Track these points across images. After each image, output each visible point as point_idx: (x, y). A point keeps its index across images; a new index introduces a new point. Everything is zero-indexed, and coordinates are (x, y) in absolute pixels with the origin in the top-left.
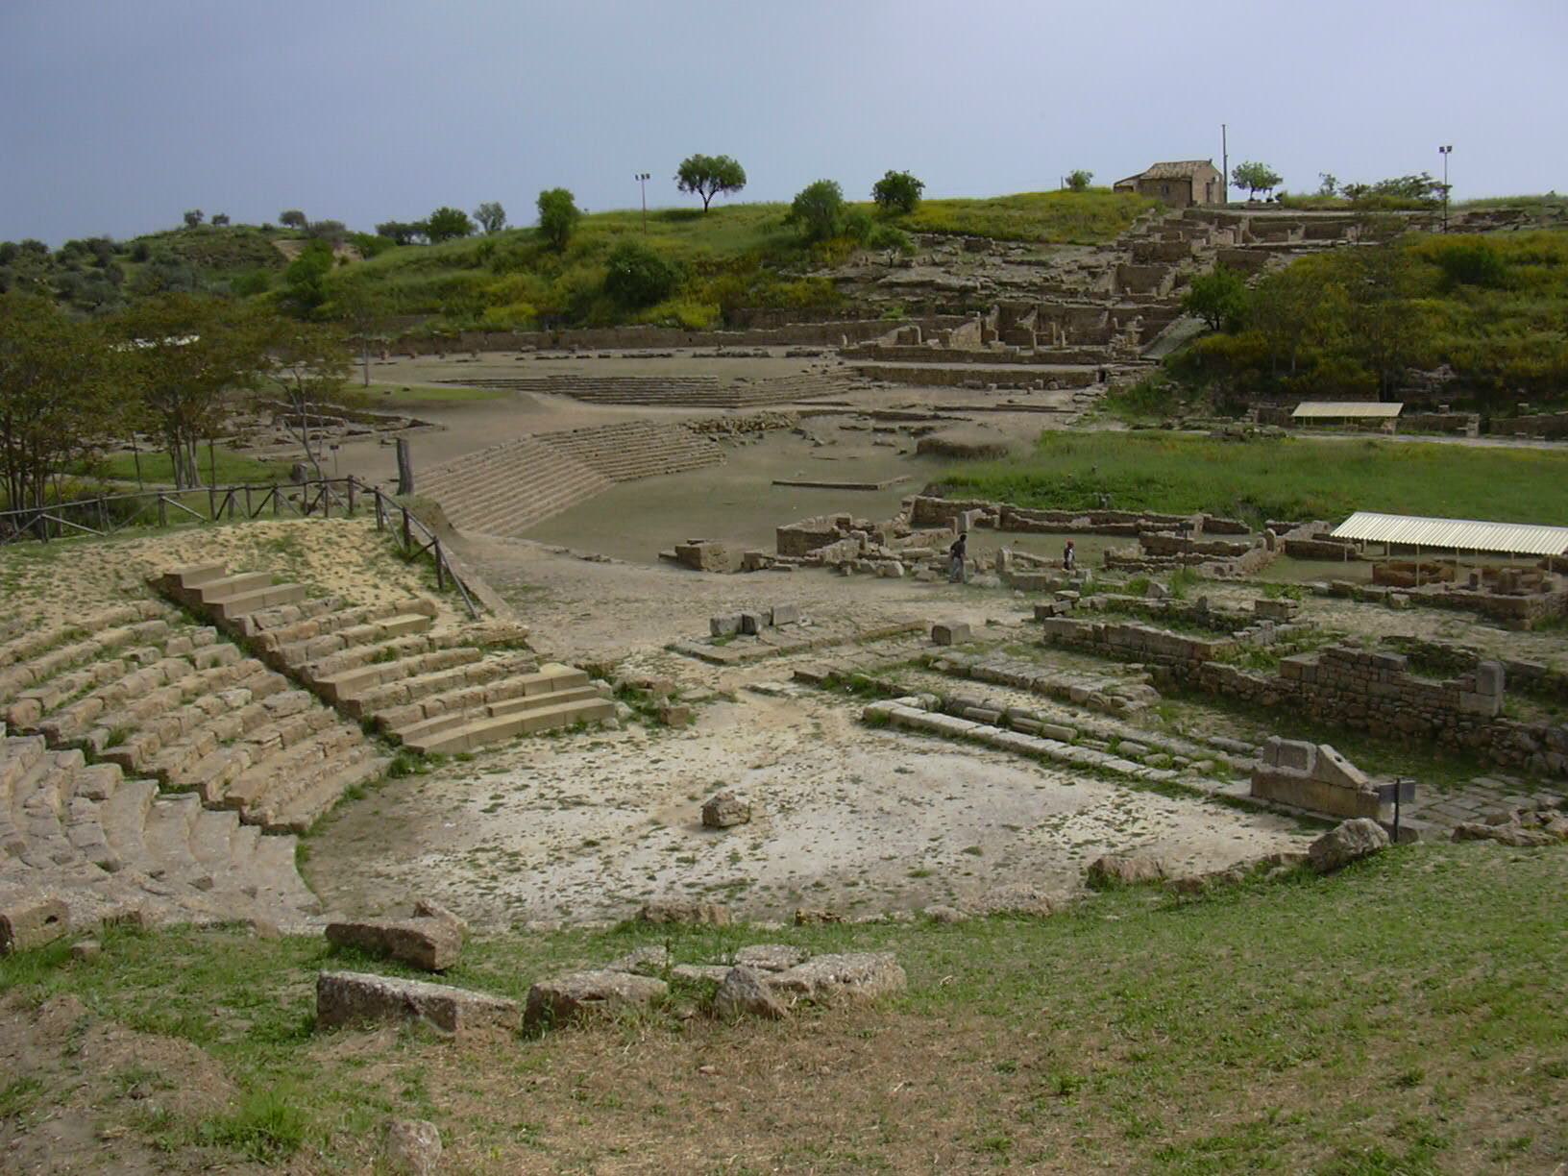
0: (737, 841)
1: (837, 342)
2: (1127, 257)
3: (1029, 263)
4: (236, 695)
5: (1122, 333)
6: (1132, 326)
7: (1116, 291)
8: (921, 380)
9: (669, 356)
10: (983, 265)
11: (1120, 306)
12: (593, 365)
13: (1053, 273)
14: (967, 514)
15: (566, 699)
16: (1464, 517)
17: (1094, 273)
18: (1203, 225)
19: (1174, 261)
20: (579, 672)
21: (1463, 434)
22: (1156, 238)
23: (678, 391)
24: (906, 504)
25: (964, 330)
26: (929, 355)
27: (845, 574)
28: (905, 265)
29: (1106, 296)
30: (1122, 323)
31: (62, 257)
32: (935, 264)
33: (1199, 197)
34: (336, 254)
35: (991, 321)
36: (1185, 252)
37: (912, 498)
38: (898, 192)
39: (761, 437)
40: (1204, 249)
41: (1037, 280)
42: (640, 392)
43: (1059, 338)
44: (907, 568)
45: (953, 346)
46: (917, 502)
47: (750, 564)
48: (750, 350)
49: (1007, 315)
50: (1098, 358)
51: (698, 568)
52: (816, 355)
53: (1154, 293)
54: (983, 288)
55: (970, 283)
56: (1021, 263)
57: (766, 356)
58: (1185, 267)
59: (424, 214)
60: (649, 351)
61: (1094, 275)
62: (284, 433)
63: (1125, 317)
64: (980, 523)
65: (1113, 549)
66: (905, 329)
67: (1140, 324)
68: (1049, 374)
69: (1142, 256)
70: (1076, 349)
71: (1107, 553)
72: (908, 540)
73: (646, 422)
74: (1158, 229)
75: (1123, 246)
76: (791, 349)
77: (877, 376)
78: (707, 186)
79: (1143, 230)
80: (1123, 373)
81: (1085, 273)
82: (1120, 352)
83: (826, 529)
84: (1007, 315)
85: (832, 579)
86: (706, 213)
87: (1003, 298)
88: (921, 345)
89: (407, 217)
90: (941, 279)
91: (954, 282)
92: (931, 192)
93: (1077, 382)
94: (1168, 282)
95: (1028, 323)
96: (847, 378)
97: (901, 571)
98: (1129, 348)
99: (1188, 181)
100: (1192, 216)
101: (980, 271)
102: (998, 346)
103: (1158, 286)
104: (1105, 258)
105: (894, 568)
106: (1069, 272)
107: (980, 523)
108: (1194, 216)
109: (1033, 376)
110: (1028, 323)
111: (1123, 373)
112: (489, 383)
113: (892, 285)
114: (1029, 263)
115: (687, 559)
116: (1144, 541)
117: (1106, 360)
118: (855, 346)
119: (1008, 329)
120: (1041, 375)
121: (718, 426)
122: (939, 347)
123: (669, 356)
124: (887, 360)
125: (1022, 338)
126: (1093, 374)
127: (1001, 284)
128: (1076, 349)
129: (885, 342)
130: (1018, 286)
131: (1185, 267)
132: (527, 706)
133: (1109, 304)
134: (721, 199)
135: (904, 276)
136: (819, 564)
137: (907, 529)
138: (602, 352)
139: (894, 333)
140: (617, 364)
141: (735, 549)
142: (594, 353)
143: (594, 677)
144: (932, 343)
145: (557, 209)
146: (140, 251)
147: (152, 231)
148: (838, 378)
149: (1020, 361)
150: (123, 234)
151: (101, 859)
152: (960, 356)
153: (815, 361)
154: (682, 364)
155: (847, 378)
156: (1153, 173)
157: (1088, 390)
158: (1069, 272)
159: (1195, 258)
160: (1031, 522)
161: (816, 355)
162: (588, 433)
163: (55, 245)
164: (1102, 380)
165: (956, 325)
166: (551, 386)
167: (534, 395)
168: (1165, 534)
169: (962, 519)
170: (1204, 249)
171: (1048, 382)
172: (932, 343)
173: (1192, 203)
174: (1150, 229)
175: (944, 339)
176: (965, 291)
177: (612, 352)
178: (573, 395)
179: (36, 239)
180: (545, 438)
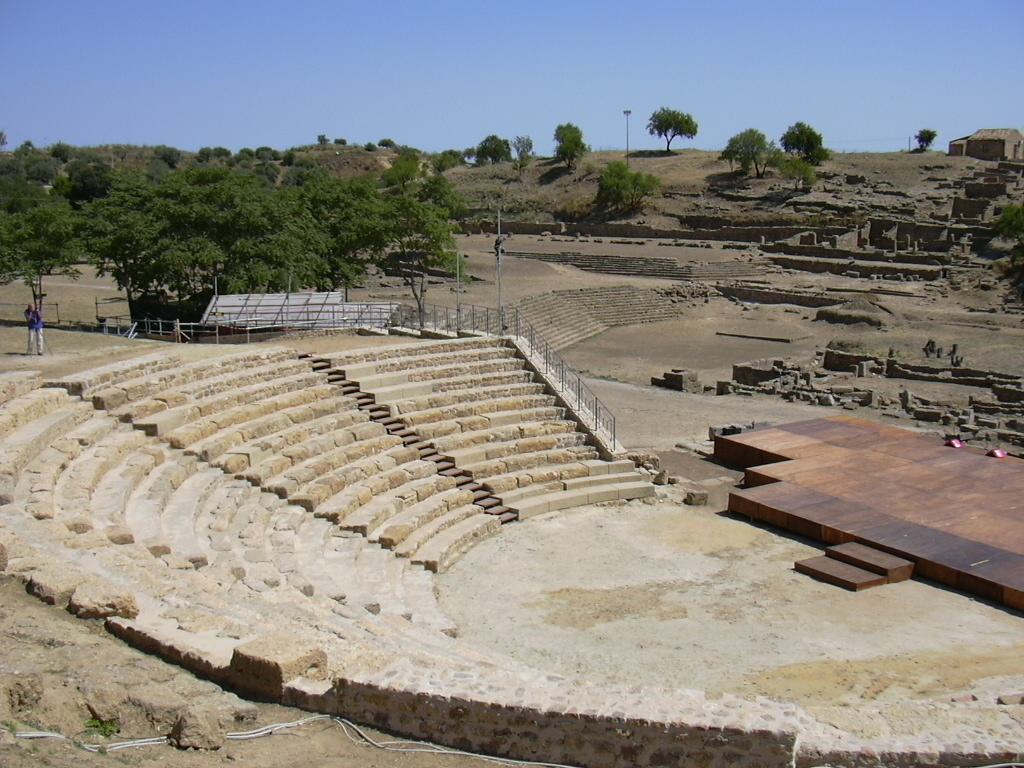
0: (42, 710)
1: (759, 241)
2: (962, 193)
3: (892, 193)
4: (382, 458)
5: (958, 244)
6: (964, 240)
7: (953, 216)
8: (816, 269)
9: (642, 243)
10: (859, 193)
11: (954, 226)
12: (588, 246)
13: (908, 201)
14: (864, 363)
15: (621, 480)
16: (768, 453)
17: (936, 201)
18: (1012, 173)
19: (994, 196)
20: (630, 461)
21: (477, 429)
22: (981, 180)
23: (651, 267)
24: (819, 354)
25: (847, 236)
26: (822, 252)
27: (791, 401)
28: (806, 191)
29: (945, 218)
30: (958, 237)
31: (238, 159)
32: (826, 191)
33: (1009, 153)
34: (19, 214)
35: (866, 232)
36: (1001, 190)
37: (823, 350)
38: (804, 141)
39: (706, 301)
40: (1015, 189)
41: (898, 205)
42: (622, 266)
43: (912, 245)
44: (837, 400)
45: (838, 247)
46: (827, 353)
47: (722, 389)
48: (698, 242)
49: (878, 227)
50: (943, 261)
51: (679, 389)
52: (744, 248)
53: (980, 218)
54: (861, 208)
55: (850, 205)
56: (885, 193)
57: (708, 246)
58: (1002, 201)
59: (475, 143)
60: (628, 240)
61: (937, 204)
62: (385, 279)
63: (960, 233)
64: (873, 370)
65: (974, 395)
66: (806, 234)
67: (970, 239)
68: (907, 270)
69: (972, 191)
70: (926, 254)
71: (971, 398)
72: (825, 379)
73: (629, 287)
74: (981, 175)
75: (958, 184)
76: (726, 243)
77: (787, 265)
78: (670, 133)
79: (971, 175)
80: (960, 272)
81: (931, 202)
82: (956, 257)
83: (768, 368)
84: (878, 227)
85: (783, 404)
86: (668, 153)
87: (876, 215)
88: (816, 245)
89: (460, 147)
90: (829, 200)
91: (840, 203)
92: (833, 141)
93: (930, 276)
94: (989, 211)
95: (892, 234)
96: (765, 265)
97: (833, 401)
98: (962, 255)
99: (1002, 143)
100: (1005, 167)
101: (858, 197)
102: (870, 249)
103: (983, 213)
104: (945, 192)
105: (827, 399)
106: (920, 201)
107: (873, 370)
108: (1005, 166)
109: (896, 271)
110: (892, 234)
111: (960, 272)
112: (520, 255)
113: (795, 204)
114: (892, 193)
115: (672, 382)
116: (995, 391)
117: (948, 263)
118: (771, 244)
119: (877, 238)
120: (902, 271)
121: (678, 293)
122: (829, 247)
123: (642, 243)
124: (793, 254)
125: (888, 244)
126: (938, 272)
127: (873, 207)
128: (926, 254)
129: (794, 241)
130: (883, 209)
131: (1002, 201)
132: (590, 484)
133: (948, 224)
134: (679, 143)
135: (804, 198)
136: (771, 392)
137: (822, 371)
138: (596, 238)
139: (798, 236)
140: (607, 246)
141: (710, 378)
142: (591, 239)
143: (638, 466)
144: (825, 244)
145: (570, 141)
146: (289, 159)
147: (297, 145)
148: (759, 265)
149: (886, 260)
150: (281, 146)
151: (301, 582)
152: (845, 254)
153: (743, 252)
154: (651, 249)
155: (765, 265)
156: (977, 137)
157: (935, 283)
158: (920, 201)
159: (1009, 196)
160: (909, 372)
161: (744, 248)
162: (591, 292)
163: (235, 151)
164: (944, 276)
165: (841, 232)
166: (563, 259)
167: (552, 265)
168: (1009, 386)
169: (861, 367)
170: (1015, 189)
171: (908, 275)
172: (825, 244)
173: (1005, 158)
174: (976, 174)
175: (833, 242)
176: (847, 211)
177: (603, 239)
178: (577, 266)
179: (224, 146)
180: (561, 293)
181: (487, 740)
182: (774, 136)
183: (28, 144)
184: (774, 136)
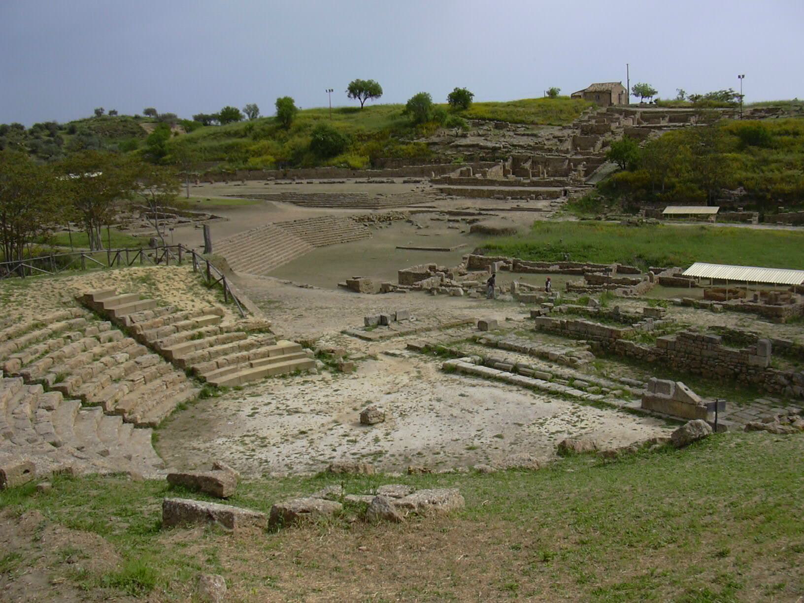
1: (429, 175)
2: (578, 132)
3: (528, 135)
4: (121, 356)
5: (575, 171)
6: (580, 167)
7: (572, 149)
8: (472, 195)
9: (343, 182)
10: (504, 136)
11: (574, 157)
12: (304, 187)
13: (540, 140)
14: (496, 263)
15: (290, 358)
17: (561, 140)
18: (617, 116)
19: (602, 134)
20: (297, 344)
22: (593, 122)
23: (348, 200)
24: (465, 258)
25: (495, 169)
26: (476, 182)
27: (433, 295)
28: (464, 136)
29: (567, 152)
30: (575, 166)
31: (32, 132)
32: (479, 135)
33: (615, 101)
35: (508, 165)
36: (607, 129)
37: (467, 256)
38: (460, 98)
39: (390, 224)
40: (617, 128)
41: (532, 144)
42: (328, 201)
43: (543, 173)
44: (465, 291)
45: (488, 177)
46: (470, 257)
47: (385, 289)
48: (385, 180)
49: (516, 161)
50: (563, 184)
51: (358, 291)
52: (418, 182)
53: (592, 150)
54: (504, 147)
55: (497, 145)
56: (524, 135)
57: (393, 182)
58: (608, 137)
59: (217, 110)
60: (333, 180)
61: (561, 141)
62: (146, 222)
63: (577, 163)
64: (503, 268)
65: (571, 282)
66: (464, 169)
67: (584, 166)
68: (538, 192)
69: (586, 131)
70: (552, 179)
71: (568, 284)
72: (465, 277)
73: (331, 216)
74: (594, 118)
75: (576, 126)
76: (406, 179)
77: (450, 193)
78: (362, 95)
79: (586, 118)
80: (576, 192)
81: (556, 140)
82: (575, 180)
83: (424, 271)
84: (516, 161)
85: (427, 297)
86: (362, 109)
87: (515, 153)
88: (472, 177)
89: (209, 111)
90: (482, 143)
91: (489, 144)
92: (477, 99)
93: (552, 196)
94: (599, 144)
95: (527, 165)
96: (434, 194)
97: (462, 293)
98: (579, 178)
99: (609, 93)
100: (611, 111)
101: (503, 139)
102: (512, 177)
103: (594, 147)
104: (566, 132)
105: (458, 291)
106: (548, 140)
107: (503, 268)
108: (612, 111)
109: (530, 193)
110: (527, 165)
111: (576, 192)
112: (251, 196)
113: (457, 146)
114: (528, 135)
115: (352, 287)
116: (587, 278)
117: (567, 185)
118: (438, 178)
119: (517, 169)
120: (534, 192)
121: (368, 219)
122: (482, 178)
123: (343, 182)
124: (455, 185)
125: (524, 173)
126: (560, 192)
127: (513, 146)
128: (552, 179)
129: (454, 175)
130: (522, 147)
131: (608, 137)
132: (270, 362)
133: (568, 156)
134: (370, 102)
135: (463, 142)
136: (420, 289)
137: (465, 271)
138: (309, 181)
139: (459, 171)
140: (316, 187)
141: (377, 281)
142: (305, 181)
143: (305, 347)
144: (478, 176)
145: (286, 107)
146: (72, 129)
147: (78, 118)
148: (430, 194)
149: (523, 185)
150: (63, 120)
152: (492, 182)
153: (418, 185)
154: (350, 186)
155: (434, 194)
156: (591, 89)
157: (558, 200)
158: (548, 140)
159: (613, 132)
160: (529, 267)
161: (418, 182)
162: (301, 222)
163: (28, 126)
164: (565, 195)
165: (490, 166)
166: (283, 198)
167: (274, 203)
168: (597, 274)
169: (493, 266)
170: (617, 128)
171: (538, 196)
172: (478, 176)
173: (611, 104)
174: (589, 117)
175: (484, 174)
176: (495, 149)
177: (314, 180)
178: (294, 203)
179: (18, 122)
180: (279, 224)
181: (713, 577)
182: (440, 98)
183: (471, 95)
184: (440, 98)
